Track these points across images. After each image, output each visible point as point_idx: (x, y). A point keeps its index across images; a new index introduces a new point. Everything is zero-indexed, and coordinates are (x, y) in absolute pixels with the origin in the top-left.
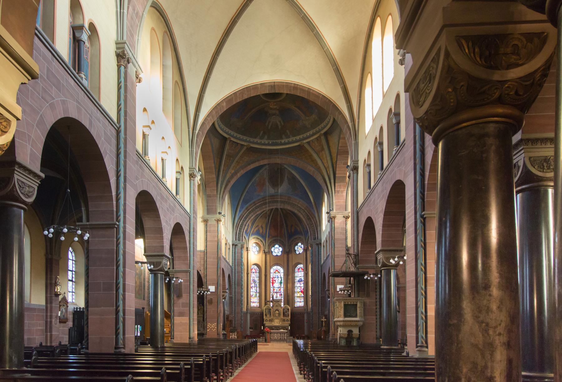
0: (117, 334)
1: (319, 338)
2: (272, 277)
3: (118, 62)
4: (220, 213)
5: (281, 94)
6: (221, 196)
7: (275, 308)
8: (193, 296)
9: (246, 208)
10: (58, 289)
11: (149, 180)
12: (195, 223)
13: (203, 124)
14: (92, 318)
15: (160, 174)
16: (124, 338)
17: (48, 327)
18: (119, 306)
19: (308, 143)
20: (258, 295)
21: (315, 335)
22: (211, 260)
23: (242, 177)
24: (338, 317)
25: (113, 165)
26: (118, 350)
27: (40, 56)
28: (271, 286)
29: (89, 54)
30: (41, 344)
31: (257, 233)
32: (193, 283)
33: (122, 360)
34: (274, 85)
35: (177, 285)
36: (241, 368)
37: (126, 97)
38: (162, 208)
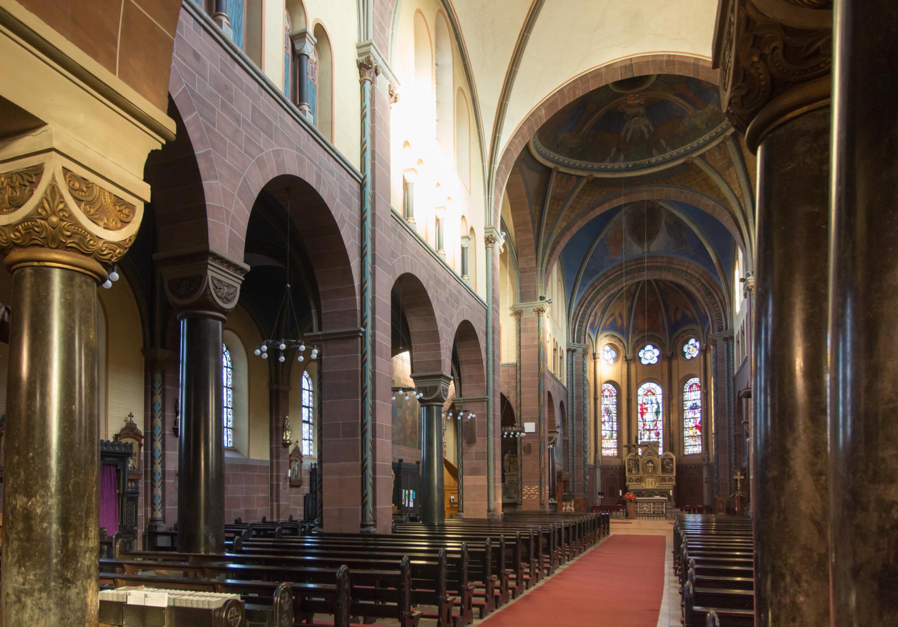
0: (364, 504)
1: (730, 511)
2: (640, 402)
3: (361, 76)
4: (542, 298)
5: (647, 76)
6: (544, 269)
7: (646, 458)
8: (494, 441)
9: (591, 285)
10: (287, 436)
11: (414, 256)
12: (496, 319)
13: (508, 151)
14: (328, 479)
15: (432, 244)
16: (375, 510)
17: (274, 493)
18: (366, 460)
19: (702, 157)
20: (615, 435)
21: (721, 506)
22: (528, 379)
23: (582, 230)
25: (354, 239)
26: (365, 529)
27: (242, 90)
28: (640, 418)
29: (317, 72)
30: (264, 518)
31: (613, 327)
32: (494, 419)
33: (372, 544)
34: (631, 65)
35: (467, 423)
36: (571, 563)
37: (373, 129)
38: (438, 299)
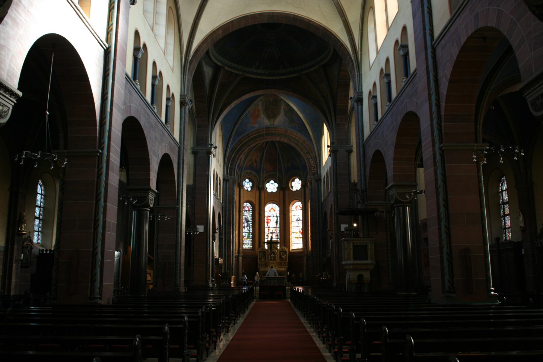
20: (251, 236)
24: (347, 260)
28: (266, 226)
